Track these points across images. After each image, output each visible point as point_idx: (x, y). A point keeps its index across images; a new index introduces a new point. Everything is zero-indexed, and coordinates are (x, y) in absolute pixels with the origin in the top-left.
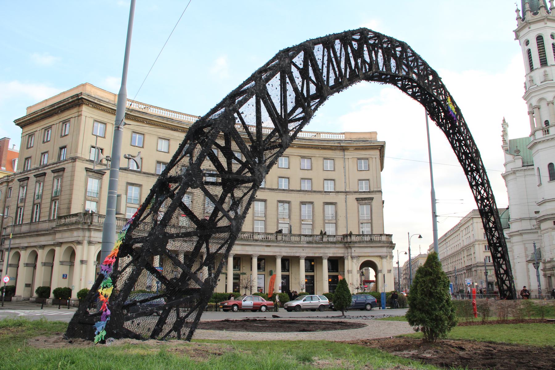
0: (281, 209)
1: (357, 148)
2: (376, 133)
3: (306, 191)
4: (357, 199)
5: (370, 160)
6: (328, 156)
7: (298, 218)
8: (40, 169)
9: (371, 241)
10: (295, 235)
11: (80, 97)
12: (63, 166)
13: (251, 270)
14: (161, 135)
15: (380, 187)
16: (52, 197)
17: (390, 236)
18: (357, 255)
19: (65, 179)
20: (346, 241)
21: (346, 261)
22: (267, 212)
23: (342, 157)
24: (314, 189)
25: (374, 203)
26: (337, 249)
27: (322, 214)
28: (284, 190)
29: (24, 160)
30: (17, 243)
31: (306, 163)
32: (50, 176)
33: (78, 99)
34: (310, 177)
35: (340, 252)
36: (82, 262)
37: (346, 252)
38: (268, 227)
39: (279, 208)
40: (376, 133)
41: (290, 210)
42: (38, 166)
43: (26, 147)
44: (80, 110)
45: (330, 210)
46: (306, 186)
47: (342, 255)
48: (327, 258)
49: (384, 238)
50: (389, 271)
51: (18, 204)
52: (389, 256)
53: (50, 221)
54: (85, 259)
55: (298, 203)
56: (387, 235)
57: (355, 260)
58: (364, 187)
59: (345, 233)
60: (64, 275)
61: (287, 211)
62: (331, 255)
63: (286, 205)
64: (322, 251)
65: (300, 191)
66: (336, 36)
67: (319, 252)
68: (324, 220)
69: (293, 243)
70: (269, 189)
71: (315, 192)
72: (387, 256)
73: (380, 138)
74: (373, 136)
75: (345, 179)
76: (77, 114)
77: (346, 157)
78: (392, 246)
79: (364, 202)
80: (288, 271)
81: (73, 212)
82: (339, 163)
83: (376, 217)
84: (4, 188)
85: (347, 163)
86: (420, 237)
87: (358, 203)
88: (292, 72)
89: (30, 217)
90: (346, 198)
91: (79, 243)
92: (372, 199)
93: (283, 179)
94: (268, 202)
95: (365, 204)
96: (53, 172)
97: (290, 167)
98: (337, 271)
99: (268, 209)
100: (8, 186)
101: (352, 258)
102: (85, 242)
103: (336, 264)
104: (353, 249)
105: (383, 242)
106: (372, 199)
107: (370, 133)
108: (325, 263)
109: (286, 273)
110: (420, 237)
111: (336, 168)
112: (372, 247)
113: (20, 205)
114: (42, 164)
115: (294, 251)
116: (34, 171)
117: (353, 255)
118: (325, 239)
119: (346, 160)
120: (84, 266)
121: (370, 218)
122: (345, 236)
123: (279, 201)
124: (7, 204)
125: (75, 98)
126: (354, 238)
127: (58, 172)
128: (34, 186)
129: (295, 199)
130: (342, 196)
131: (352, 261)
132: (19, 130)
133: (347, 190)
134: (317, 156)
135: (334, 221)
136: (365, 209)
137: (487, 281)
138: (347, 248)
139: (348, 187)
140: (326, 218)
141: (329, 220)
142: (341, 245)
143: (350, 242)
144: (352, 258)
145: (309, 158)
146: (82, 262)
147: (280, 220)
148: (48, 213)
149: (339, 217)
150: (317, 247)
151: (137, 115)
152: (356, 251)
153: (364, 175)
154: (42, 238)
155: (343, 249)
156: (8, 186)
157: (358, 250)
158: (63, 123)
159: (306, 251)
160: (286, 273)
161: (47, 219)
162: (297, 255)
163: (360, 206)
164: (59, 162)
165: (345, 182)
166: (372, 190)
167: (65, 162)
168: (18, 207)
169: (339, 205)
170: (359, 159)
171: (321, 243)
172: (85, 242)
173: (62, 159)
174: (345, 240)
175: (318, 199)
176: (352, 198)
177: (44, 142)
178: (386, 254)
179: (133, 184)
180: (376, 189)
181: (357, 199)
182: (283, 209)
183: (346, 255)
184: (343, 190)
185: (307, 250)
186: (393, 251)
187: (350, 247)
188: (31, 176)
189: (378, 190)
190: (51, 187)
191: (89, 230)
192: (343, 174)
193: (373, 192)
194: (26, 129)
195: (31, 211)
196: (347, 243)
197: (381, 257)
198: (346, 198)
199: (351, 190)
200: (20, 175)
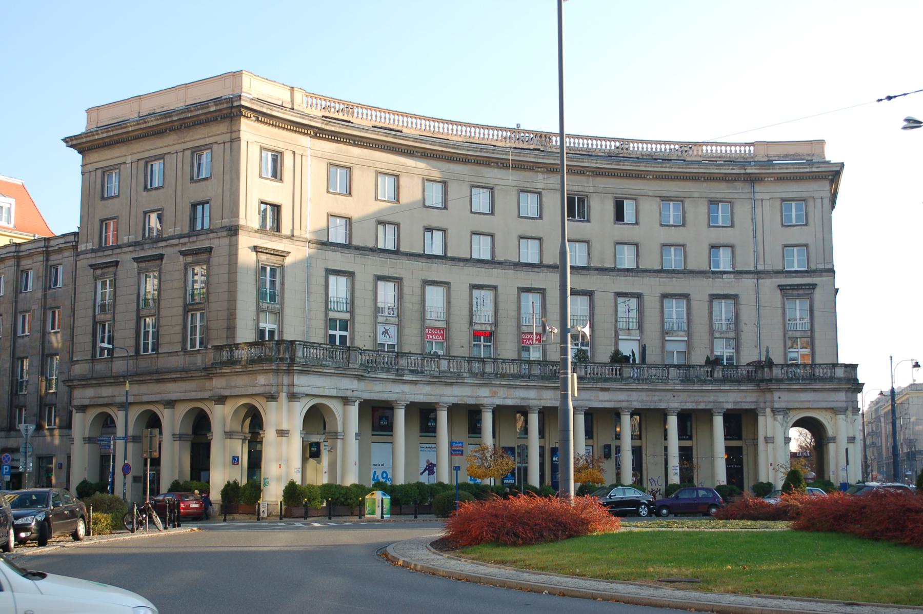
0: (621, 308)
1: (782, 178)
2: (821, 143)
3: (673, 272)
4: (782, 288)
5: (811, 203)
6: (718, 196)
7: (658, 328)
8: (146, 246)
9: (813, 378)
10: (651, 366)
11: (235, 104)
12: (206, 244)
13: (666, 439)
14: (382, 167)
16: (185, 305)
17: (854, 367)
20: (761, 374)
21: (761, 419)
22: (595, 317)
23: (748, 196)
24: (690, 267)
25: (818, 294)
27: (706, 320)
28: (627, 270)
30: (104, 395)
31: (672, 213)
32: (174, 262)
33: (232, 107)
34: (681, 242)
36: (767, 440)
39: (619, 309)
40: (821, 143)
41: (641, 311)
42: (140, 239)
43: (98, 195)
44: (234, 128)
45: (723, 310)
46: (673, 261)
47: (753, 407)
48: (722, 411)
49: (840, 373)
50: (852, 440)
51: (94, 316)
52: (850, 408)
56: (846, 366)
57: (780, 417)
58: (796, 262)
59: (755, 358)
60: (234, 458)
61: (634, 314)
62: (730, 406)
63: (633, 302)
64: (712, 397)
65: (661, 271)
67: (706, 399)
68: (711, 331)
69: (652, 383)
70: (597, 269)
71: (692, 272)
72: (846, 409)
73: (832, 155)
75: (756, 244)
76: (227, 137)
77: (758, 196)
78: (858, 387)
79: (795, 292)
80: (690, 438)
82: (742, 211)
83: (821, 325)
84: (8, 271)
86: (917, 365)
87: (783, 296)
90: (757, 285)
91: (272, 397)
92: (813, 286)
93: (626, 247)
94: (597, 296)
95: (799, 297)
96: (184, 253)
97: (641, 221)
98: (740, 438)
99: (597, 311)
101: (775, 411)
102: (283, 396)
103: (739, 423)
104: (776, 395)
105: (840, 379)
106: (813, 286)
109: (687, 443)
110: (917, 365)
111: (736, 220)
112: (815, 390)
113: (100, 317)
115: (656, 398)
116: (131, 249)
117: (776, 405)
118: (718, 374)
119: (758, 204)
121: (808, 327)
122: (758, 365)
123: (619, 294)
125: (225, 106)
126: (777, 372)
127: (196, 254)
129: (651, 287)
130: (748, 282)
131: (775, 419)
132: (75, 158)
133: (760, 268)
134: (696, 195)
135: (733, 335)
136: (798, 309)
138: (763, 391)
140: (715, 327)
141: (721, 332)
142: (750, 387)
143: (770, 380)
144: (775, 411)
145: (680, 200)
146: (767, 440)
147: (620, 333)
148: (179, 338)
149: (742, 326)
150: (702, 391)
151: (337, 129)
152: (782, 398)
153: (796, 235)
154: (170, 386)
155: (755, 394)
156: (18, 266)
157: (785, 396)
158: (193, 153)
160: (687, 443)
162: (663, 406)
163: (787, 302)
164: (193, 232)
165: (755, 252)
166: (813, 267)
168: (95, 323)
169: (743, 300)
170: (783, 200)
171: (711, 382)
172: (283, 396)
174: (760, 375)
175: (700, 289)
176: (769, 285)
178: (844, 405)
179: (338, 273)
180: (821, 267)
181: (782, 288)
182: (627, 310)
183: (762, 405)
184: (752, 269)
185: (683, 396)
186: (859, 395)
187: (770, 391)
188: (126, 257)
189: (827, 267)
190: (181, 284)
191: (290, 372)
192: (751, 234)
193: (815, 271)
194: (94, 156)
196: (762, 380)
197: (835, 411)
198: (757, 285)
199: (769, 268)
200: (93, 255)
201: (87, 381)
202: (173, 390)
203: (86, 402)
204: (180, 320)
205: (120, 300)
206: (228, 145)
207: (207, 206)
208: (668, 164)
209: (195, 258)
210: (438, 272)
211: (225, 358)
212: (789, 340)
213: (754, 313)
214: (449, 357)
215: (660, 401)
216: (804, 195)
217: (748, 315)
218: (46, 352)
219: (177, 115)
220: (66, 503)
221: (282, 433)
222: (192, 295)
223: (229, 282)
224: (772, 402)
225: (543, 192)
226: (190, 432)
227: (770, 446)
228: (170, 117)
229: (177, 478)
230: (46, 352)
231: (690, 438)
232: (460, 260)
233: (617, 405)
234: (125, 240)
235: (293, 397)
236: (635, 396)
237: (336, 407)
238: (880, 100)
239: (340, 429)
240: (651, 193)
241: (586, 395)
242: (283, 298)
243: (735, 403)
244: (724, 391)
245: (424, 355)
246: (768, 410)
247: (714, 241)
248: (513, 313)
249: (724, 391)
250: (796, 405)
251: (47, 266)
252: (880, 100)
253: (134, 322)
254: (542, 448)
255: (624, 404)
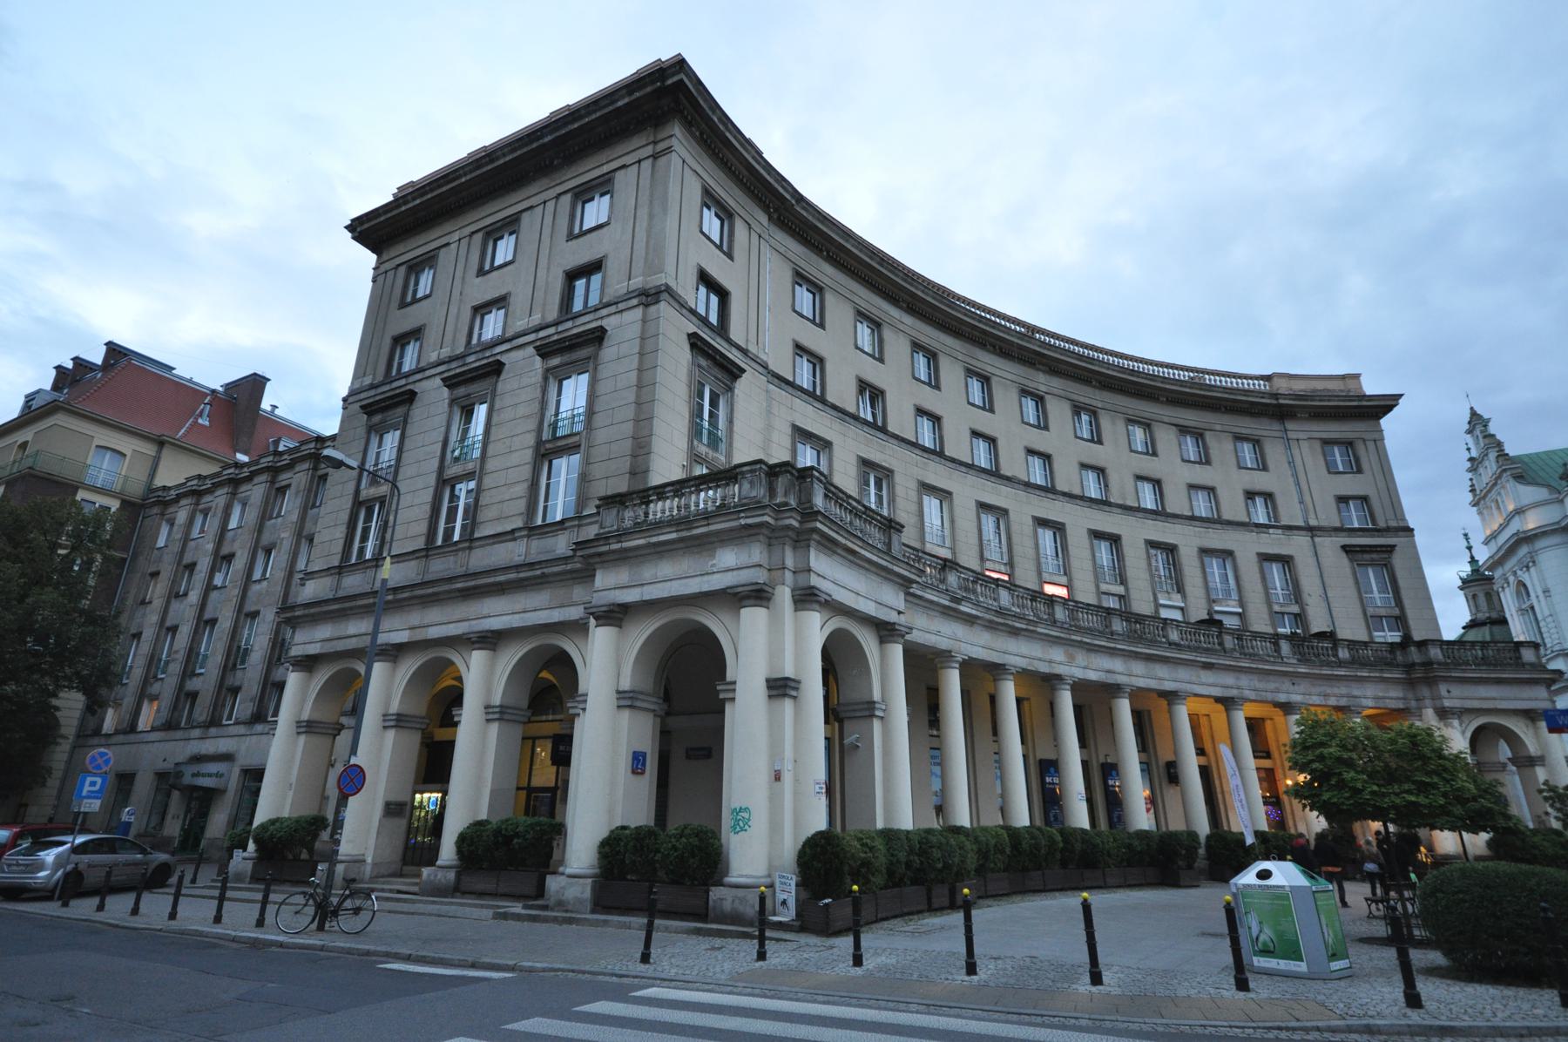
6: (1244, 431)
15: (1404, 519)
16: (539, 443)
18: (1457, 703)
19: (605, 371)
25: (1398, 560)
29: (387, 342)
32: (524, 368)
35: (1393, 694)
40: (1357, 377)
46: (1202, 507)
51: (357, 492)
53: (532, 531)
54: (789, 672)
55: (1195, 552)
74: (1351, 384)
76: (649, 150)
79: (1367, 556)
81: (656, 479)
85: (1296, 452)
89: (422, 528)
100: (273, 482)
102: (784, 595)
104: (1443, 689)
107: (1343, 377)
112: (1499, 682)
114: (475, 341)
117: (1447, 703)
120: (788, 704)
124: (266, 539)
128: (444, 417)
134: (1218, 427)
139: (1312, 515)
148: (521, 505)
153: (1350, 485)
156: (273, 482)
157: (1457, 690)
160: (1266, 763)
161: (519, 523)
165: (1301, 502)
167: (604, 312)
172: (784, 595)
173: (578, 306)
176: (1330, 546)
177: (481, 272)
181: (1345, 548)
184: (1301, 523)
191: (801, 540)
195: (428, 508)
201: (319, 612)
202: (498, 613)
203: (313, 649)
204: (526, 472)
205: (405, 472)
206: (646, 165)
207: (596, 279)
209: (566, 358)
210: (937, 474)
211: (628, 523)
212: (1373, 621)
213: (1318, 581)
214: (1011, 586)
215: (1277, 691)
216: (1350, 436)
217: (1310, 583)
218: (291, 601)
219: (551, 133)
221: (780, 688)
222: (554, 426)
223: (640, 386)
225: (1047, 397)
226: (525, 703)
228: (538, 139)
229: (483, 816)
230: (291, 601)
232: (962, 463)
234: (433, 357)
235: (807, 597)
237: (868, 641)
239: (877, 696)
240: (1166, 419)
242: (730, 445)
245: (980, 577)
247: (1249, 487)
248: (1031, 552)
251: (313, 476)
253: (431, 491)
254: (1085, 764)
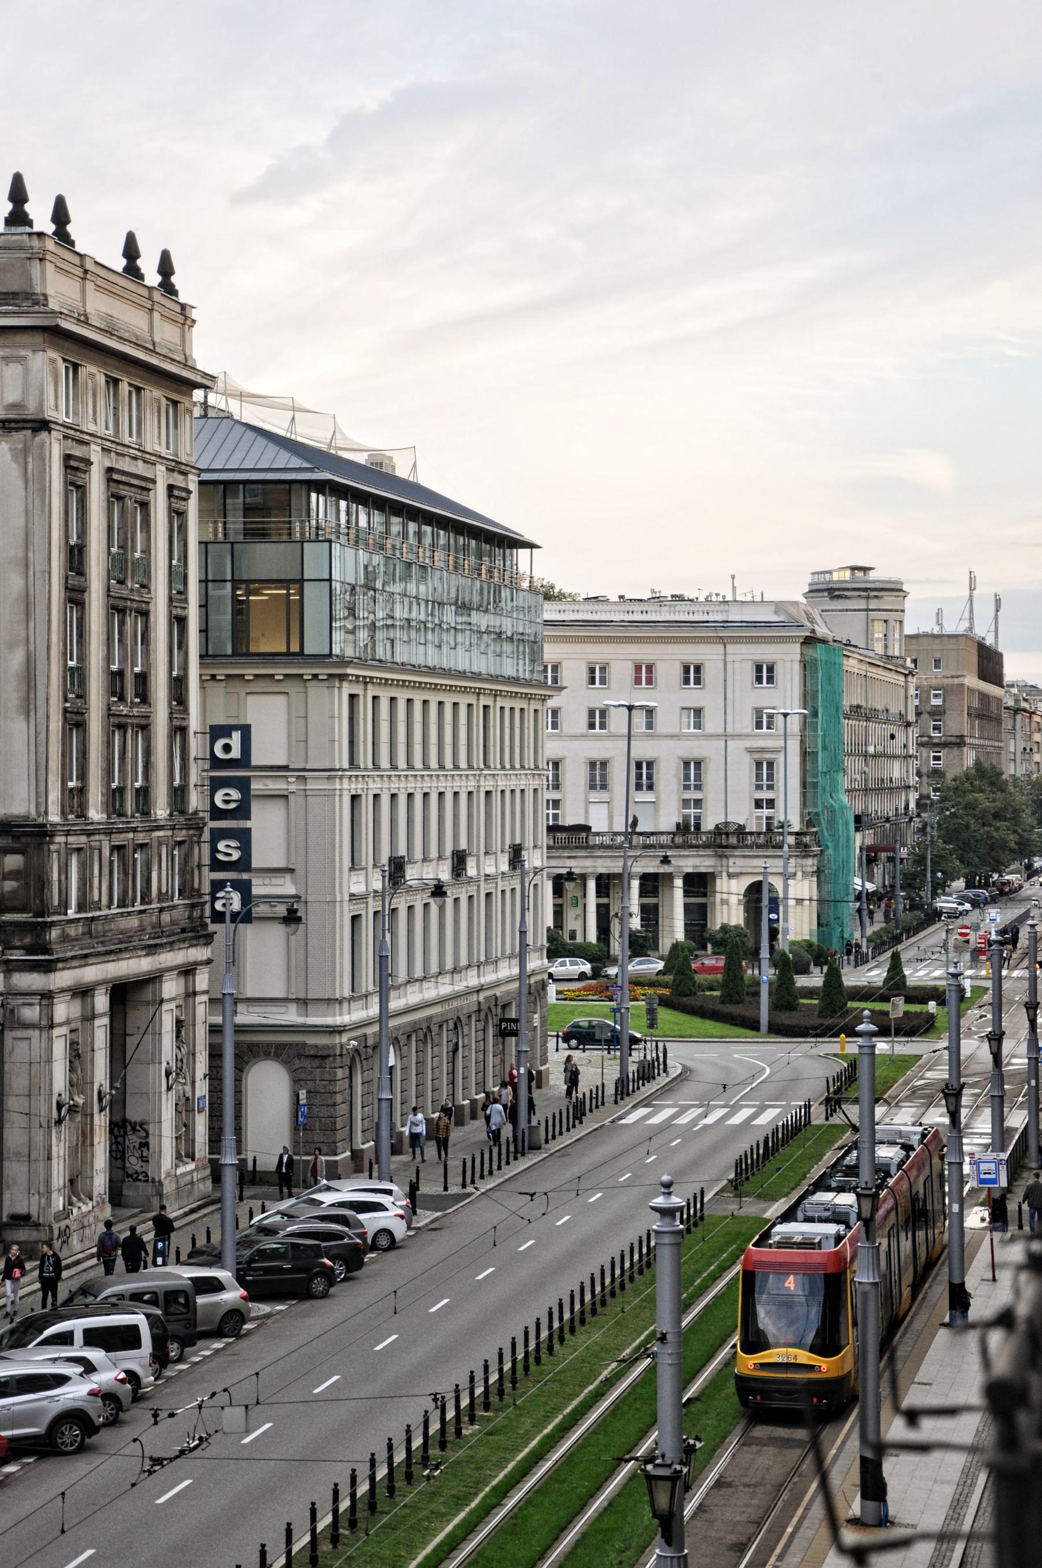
21: (718, 881)
26: (701, 859)
35: (707, 864)
37: (719, 863)
38: (310, 991)
47: (711, 870)
62: (690, 870)
66: (693, 760)
80: (608, 896)
88: (969, 1305)
101: (730, 876)
103: (699, 884)
104: (731, 861)
108: (679, 883)
109: (604, 901)
117: (731, 870)
137: (244, 504)
142: (709, 852)
152: (736, 863)
157: (740, 862)
159: (643, 864)
160: (604, 901)
183: (719, 869)
187: (726, 857)
208: (681, 606)
220: (477, 1469)
224: (728, 866)
227: (725, 907)
231: (608, 896)
233: (583, 871)
236: (600, 862)
238: (733, 577)
241: (554, 863)
243: (695, 867)
244: (684, 856)
246: (724, 874)
249: (684, 856)
250: (750, 870)
252: (733, 577)
255: (590, 870)
